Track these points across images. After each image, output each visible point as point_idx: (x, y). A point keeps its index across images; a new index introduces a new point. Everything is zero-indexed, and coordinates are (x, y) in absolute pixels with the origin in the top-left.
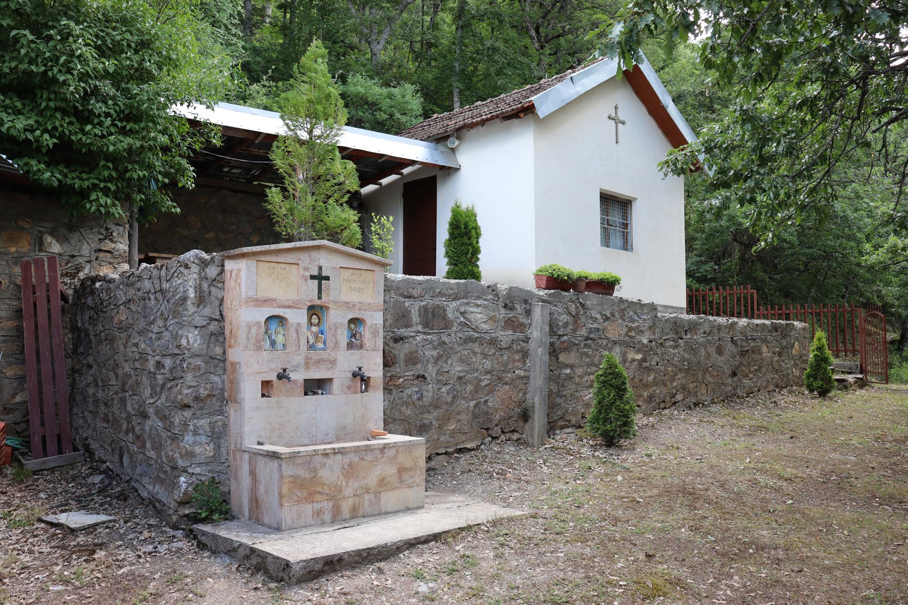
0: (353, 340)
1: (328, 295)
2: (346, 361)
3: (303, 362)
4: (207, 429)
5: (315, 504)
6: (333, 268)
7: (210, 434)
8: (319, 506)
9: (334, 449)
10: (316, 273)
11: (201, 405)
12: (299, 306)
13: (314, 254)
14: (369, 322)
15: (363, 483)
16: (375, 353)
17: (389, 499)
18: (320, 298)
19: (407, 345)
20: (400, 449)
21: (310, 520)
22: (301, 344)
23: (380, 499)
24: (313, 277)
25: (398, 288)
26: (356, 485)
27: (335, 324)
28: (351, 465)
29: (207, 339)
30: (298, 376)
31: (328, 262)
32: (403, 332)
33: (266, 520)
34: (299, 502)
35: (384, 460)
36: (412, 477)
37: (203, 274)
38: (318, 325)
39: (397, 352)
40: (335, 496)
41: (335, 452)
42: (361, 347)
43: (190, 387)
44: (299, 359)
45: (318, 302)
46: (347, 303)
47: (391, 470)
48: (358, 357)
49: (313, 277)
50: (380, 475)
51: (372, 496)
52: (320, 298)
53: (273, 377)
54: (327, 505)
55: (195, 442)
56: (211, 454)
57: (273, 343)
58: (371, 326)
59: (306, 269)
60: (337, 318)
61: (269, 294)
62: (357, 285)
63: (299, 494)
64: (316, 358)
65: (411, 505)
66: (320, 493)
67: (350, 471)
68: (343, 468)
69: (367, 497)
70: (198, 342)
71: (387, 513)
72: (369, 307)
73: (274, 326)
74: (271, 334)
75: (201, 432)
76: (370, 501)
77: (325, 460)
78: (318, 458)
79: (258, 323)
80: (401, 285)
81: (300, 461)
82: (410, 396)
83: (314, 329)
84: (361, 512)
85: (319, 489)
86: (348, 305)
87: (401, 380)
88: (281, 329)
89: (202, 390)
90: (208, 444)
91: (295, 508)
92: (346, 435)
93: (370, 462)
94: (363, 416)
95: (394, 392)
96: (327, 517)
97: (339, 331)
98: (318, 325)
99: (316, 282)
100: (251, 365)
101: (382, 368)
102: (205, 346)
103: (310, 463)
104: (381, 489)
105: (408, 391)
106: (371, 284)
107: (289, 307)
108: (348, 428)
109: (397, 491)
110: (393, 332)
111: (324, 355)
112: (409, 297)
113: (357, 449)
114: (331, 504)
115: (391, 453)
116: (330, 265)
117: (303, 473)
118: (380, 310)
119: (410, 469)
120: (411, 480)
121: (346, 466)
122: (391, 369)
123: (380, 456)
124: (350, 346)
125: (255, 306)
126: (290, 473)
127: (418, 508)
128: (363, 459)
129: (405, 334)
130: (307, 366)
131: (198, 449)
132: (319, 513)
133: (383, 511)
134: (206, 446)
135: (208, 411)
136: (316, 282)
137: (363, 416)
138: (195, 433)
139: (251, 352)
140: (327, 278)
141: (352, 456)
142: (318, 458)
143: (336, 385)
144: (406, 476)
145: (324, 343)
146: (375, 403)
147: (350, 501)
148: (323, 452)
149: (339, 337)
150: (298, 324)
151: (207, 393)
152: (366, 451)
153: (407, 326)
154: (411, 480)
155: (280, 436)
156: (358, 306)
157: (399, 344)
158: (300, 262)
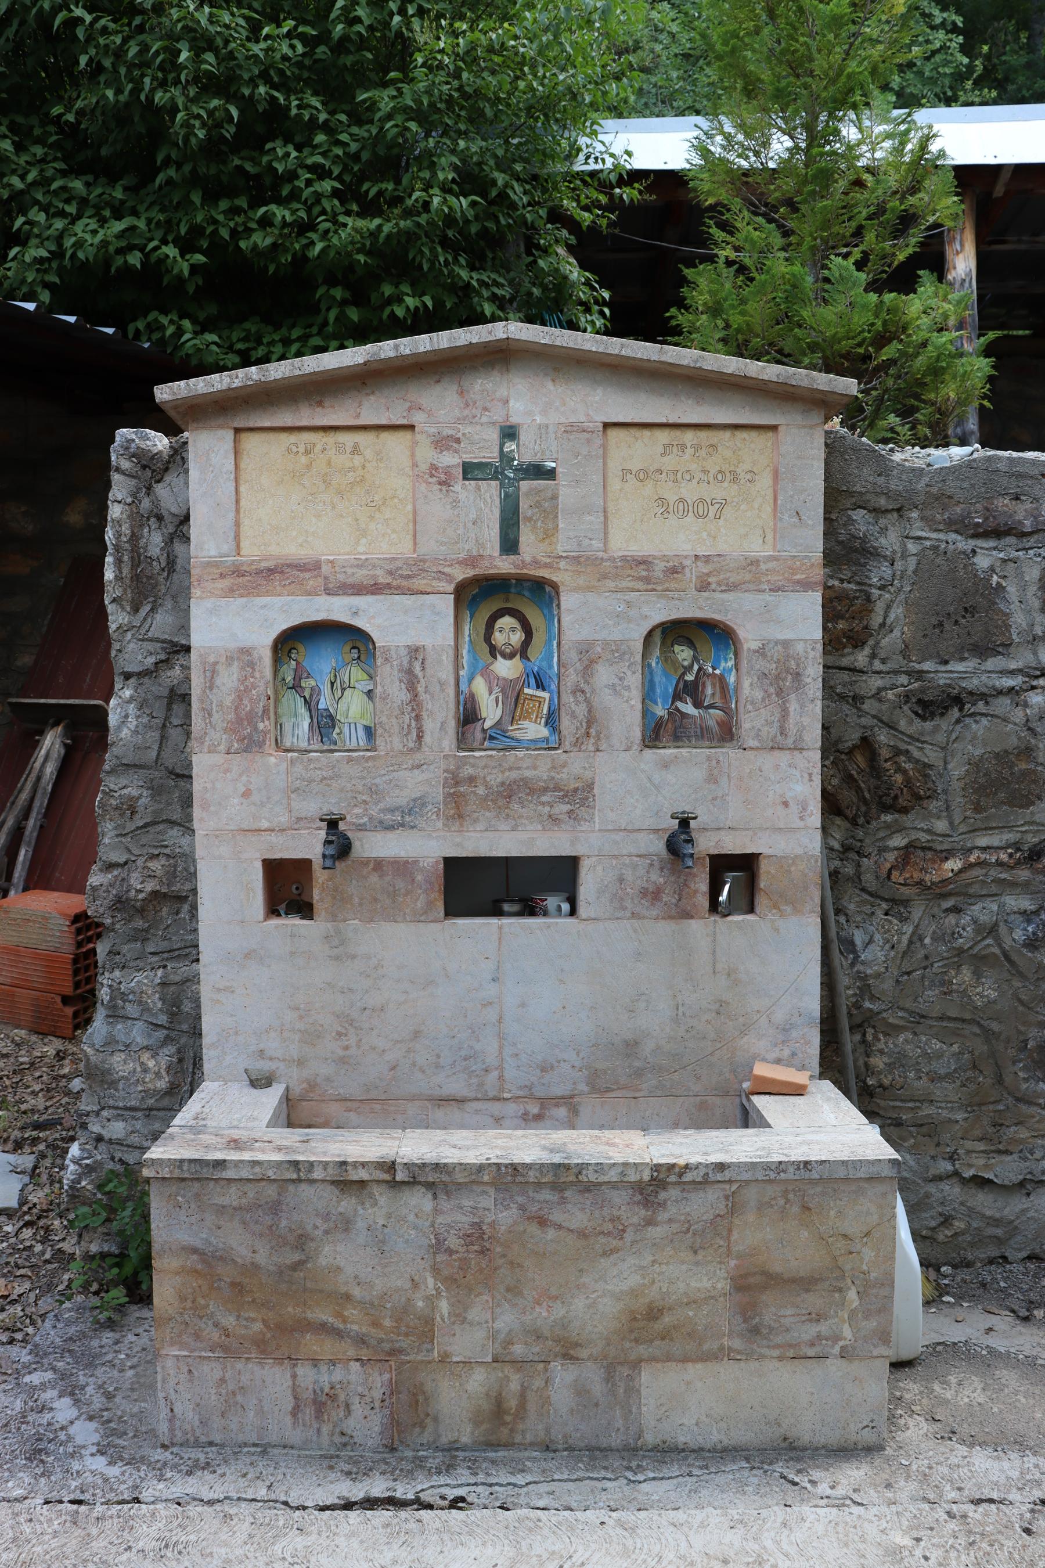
0: (688, 708)
1: (549, 535)
2: (626, 798)
3: (438, 794)
4: (155, 1002)
5: (305, 1372)
6: (570, 429)
7: (162, 1019)
8: (326, 1378)
9: (390, 1167)
11: (139, 923)
12: (419, 583)
13: (484, 386)
14: (749, 636)
15: (544, 1315)
16: (783, 758)
17: (683, 1398)
18: (510, 545)
19: (979, 727)
20: (751, 1194)
21: (281, 1425)
22: (428, 725)
23: (633, 1390)
25: (942, 499)
26: (507, 1320)
27: (585, 649)
28: (478, 1237)
29: (160, 713)
31: (538, 410)
32: (965, 672)
34: (228, 1349)
35: (656, 1232)
36: (819, 1318)
37: (146, 504)
38: (523, 651)
39: (931, 755)
40: (401, 1348)
41: (393, 1177)
42: (727, 733)
43: (110, 866)
44: (420, 782)
45: (505, 566)
46: (644, 562)
47: (694, 1281)
48: (698, 774)
50: (634, 1293)
51: (593, 1375)
52: (510, 545)
53: (310, 845)
54: (362, 1383)
55: (110, 1041)
56: (162, 1084)
57: (325, 725)
58: (761, 652)
60: (599, 623)
61: (291, 548)
62: (690, 492)
63: (229, 1321)
64: (495, 778)
65: (806, 1430)
66: (323, 1328)
67: (475, 1261)
68: (438, 1245)
69: (563, 1375)
70: (132, 722)
71: (668, 1454)
72: (751, 574)
73: (322, 663)
74: (316, 691)
75: (132, 1010)
76: (581, 1391)
77: (347, 1204)
78: (314, 1199)
79: (246, 651)
80: (952, 486)
81: (231, 1197)
82: (992, 930)
83: (506, 668)
84: (533, 1428)
85: (323, 1315)
87: (953, 864)
88: (356, 674)
89: (135, 880)
90: (153, 1050)
91: (211, 1371)
92: (639, 1073)
93: (582, 1234)
94: (721, 1007)
95: (917, 912)
96: (366, 1425)
97: (604, 675)
98: (523, 651)
100: (241, 810)
101: (815, 819)
102: (154, 736)
103: (275, 1208)
104: (642, 1350)
105: (984, 911)
106: (765, 481)
107: (375, 589)
108: (648, 1047)
109: (727, 1371)
110: (919, 675)
111: (538, 767)
112: (997, 533)
113: (509, 1177)
114: (379, 1381)
115: (703, 1205)
116: (554, 418)
117: (240, 1243)
118: (806, 586)
119: (805, 1283)
120: (811, 1331)
121: (453, 1242)
122: (907, 820)
123: (635, 1216)
124: (656, 733)
125: (231, 592)
126: (184, 1237)
127: (845, 1452)
128: (543, 1222)
129: (973, 683)
130: (457, 803)
131: (120, 1064)
132: (323, 1403)
133: (650, 1438)
134: (145, 1056)
135: (164, 945)
136: (491, 490)
137: (721, 1007)
138: (115, 1015)
139: (218, 759)
140: (539, 472)
141: (487, 1202)
142: (314, 1199)
143: (590, 884)
144: (779, 1311)
145: (552, 720)
146: (780, 960)
147: (477, 1381)
148: (332, 1173)
149: (605, 699)
150: (415, 651)
151: (150, 886)
152: (557, 1187)
153: (983, 650)
154: (811, 1331)
155: (342, 1061)
156: (691, 576)
157: (944, 724)
158: (418, 418)
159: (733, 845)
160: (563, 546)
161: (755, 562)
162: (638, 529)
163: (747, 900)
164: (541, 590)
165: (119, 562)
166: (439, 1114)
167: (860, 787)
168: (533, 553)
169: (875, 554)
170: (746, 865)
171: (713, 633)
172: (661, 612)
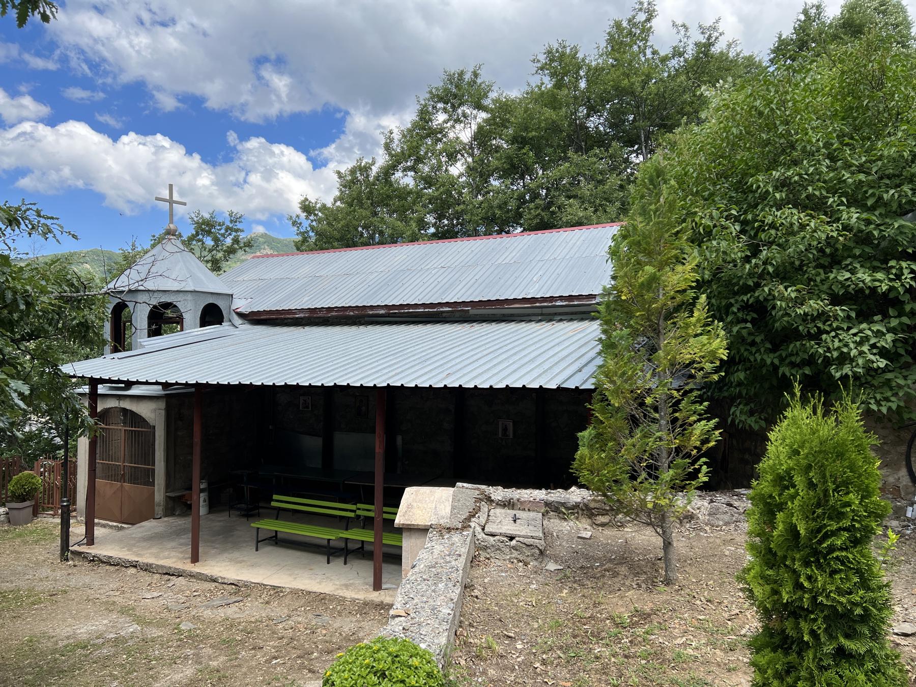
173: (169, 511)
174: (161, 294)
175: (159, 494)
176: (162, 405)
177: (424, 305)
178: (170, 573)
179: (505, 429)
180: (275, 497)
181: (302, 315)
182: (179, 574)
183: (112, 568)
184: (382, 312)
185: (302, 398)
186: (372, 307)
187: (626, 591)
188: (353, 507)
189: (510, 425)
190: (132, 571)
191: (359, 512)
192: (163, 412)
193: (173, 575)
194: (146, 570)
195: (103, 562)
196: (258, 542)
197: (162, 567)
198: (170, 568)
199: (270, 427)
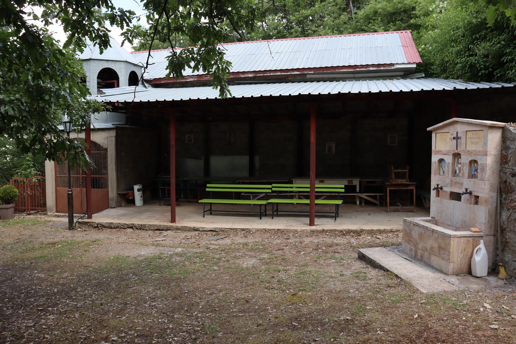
1: (460, 148)
10: (455, 136)
24: (454, 138)
30: (448, 189)
33: (473, 274)
36: (444, 254)
44: (448, 181)
45: (456, 152)
49: (454, 138)
59: (452, 134)
60: (465, 159)
62: (475, 140)
86: (469, 153)
97: (465, 167)
99: (455, 140)
110: (513, 169)
159: (477, 194)
160: (462, 149)
161: (480, 151)
162: (471, 147)
163: (476, 203)
164: (459, 154)
165: (291, 226)
166: (448, 227)
167: (503, 189)
168: (459, 150)
169: (510, 148)
170: (477, 197)
171: (475, 162)
172: (470, 159)
173: (119, 205)
174: (105, 62)
175: (112, 192)
176: (113, 133)
177: (281, 71)
178: (159, 229)
179: (330, 148)
180: (208, 185)
181: (192, 80)
182: (168, 229)
183: (114, 230)
184: (251, 75)
185: (187, 136)
186: (244, 73)
187: (163, 308)
188: (270, 186)
189: (333, 146)
190: (131, 230)
191: (274, 189)
192: (114, 139)
193: (162, 230)
194: (140, 229)
195: (106, 227)
196: (205, 212)
197: (154, 225)
198: (160, 225)
199: (165, 155)
